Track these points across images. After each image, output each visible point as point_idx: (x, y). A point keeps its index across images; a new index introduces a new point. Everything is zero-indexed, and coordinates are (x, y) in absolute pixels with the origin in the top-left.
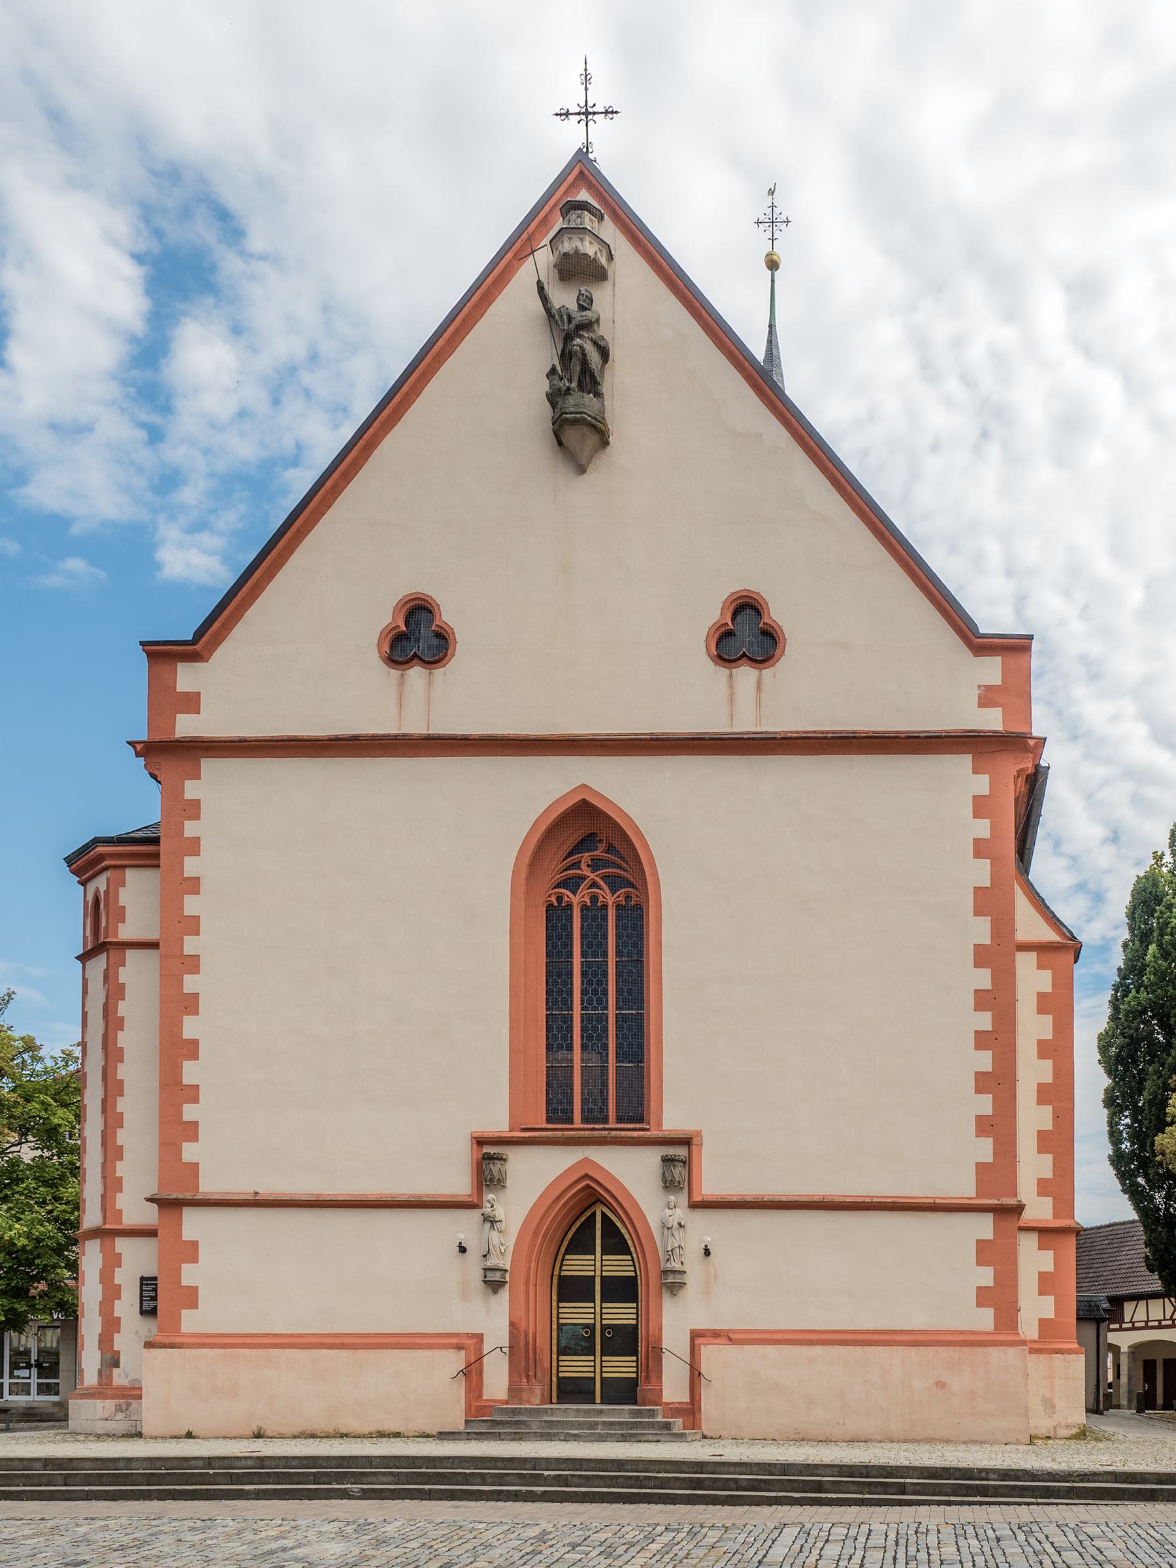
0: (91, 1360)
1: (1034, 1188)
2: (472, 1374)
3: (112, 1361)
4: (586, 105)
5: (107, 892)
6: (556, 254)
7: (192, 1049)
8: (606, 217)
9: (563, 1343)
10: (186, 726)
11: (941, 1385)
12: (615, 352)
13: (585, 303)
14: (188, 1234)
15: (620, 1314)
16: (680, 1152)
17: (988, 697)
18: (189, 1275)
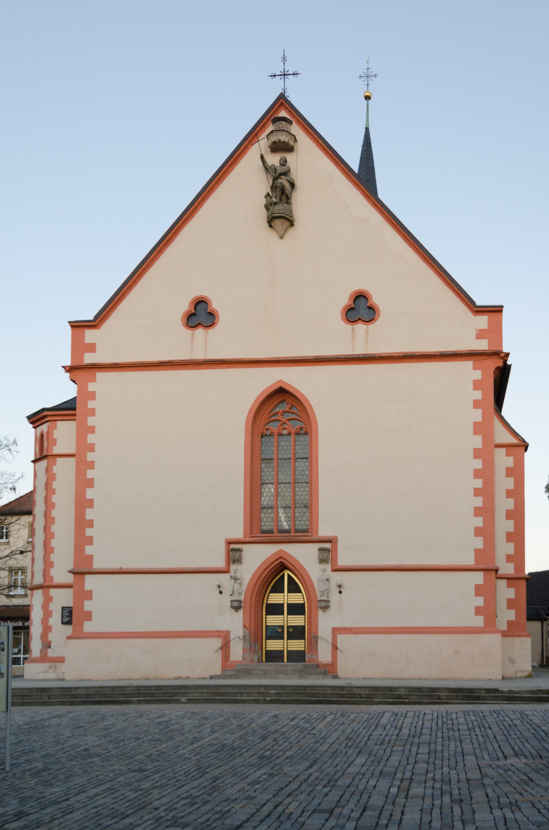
0: (36, 646)
1: (504, 559)
2: (225, 647)
3: (47, 645)
4: (284, 79)
5: (47, 432)
6: (270, 141)
7: (90, 503)
8: (294, 123)
9: (268, 634)
10: (89, 358)
11: (457, 652)
12: (298, 184)
13: (284, 162)
14: (87, 587)
15: (297, 620)
16: (328, 546)
17: (481, 334)
18: (88, 605)
